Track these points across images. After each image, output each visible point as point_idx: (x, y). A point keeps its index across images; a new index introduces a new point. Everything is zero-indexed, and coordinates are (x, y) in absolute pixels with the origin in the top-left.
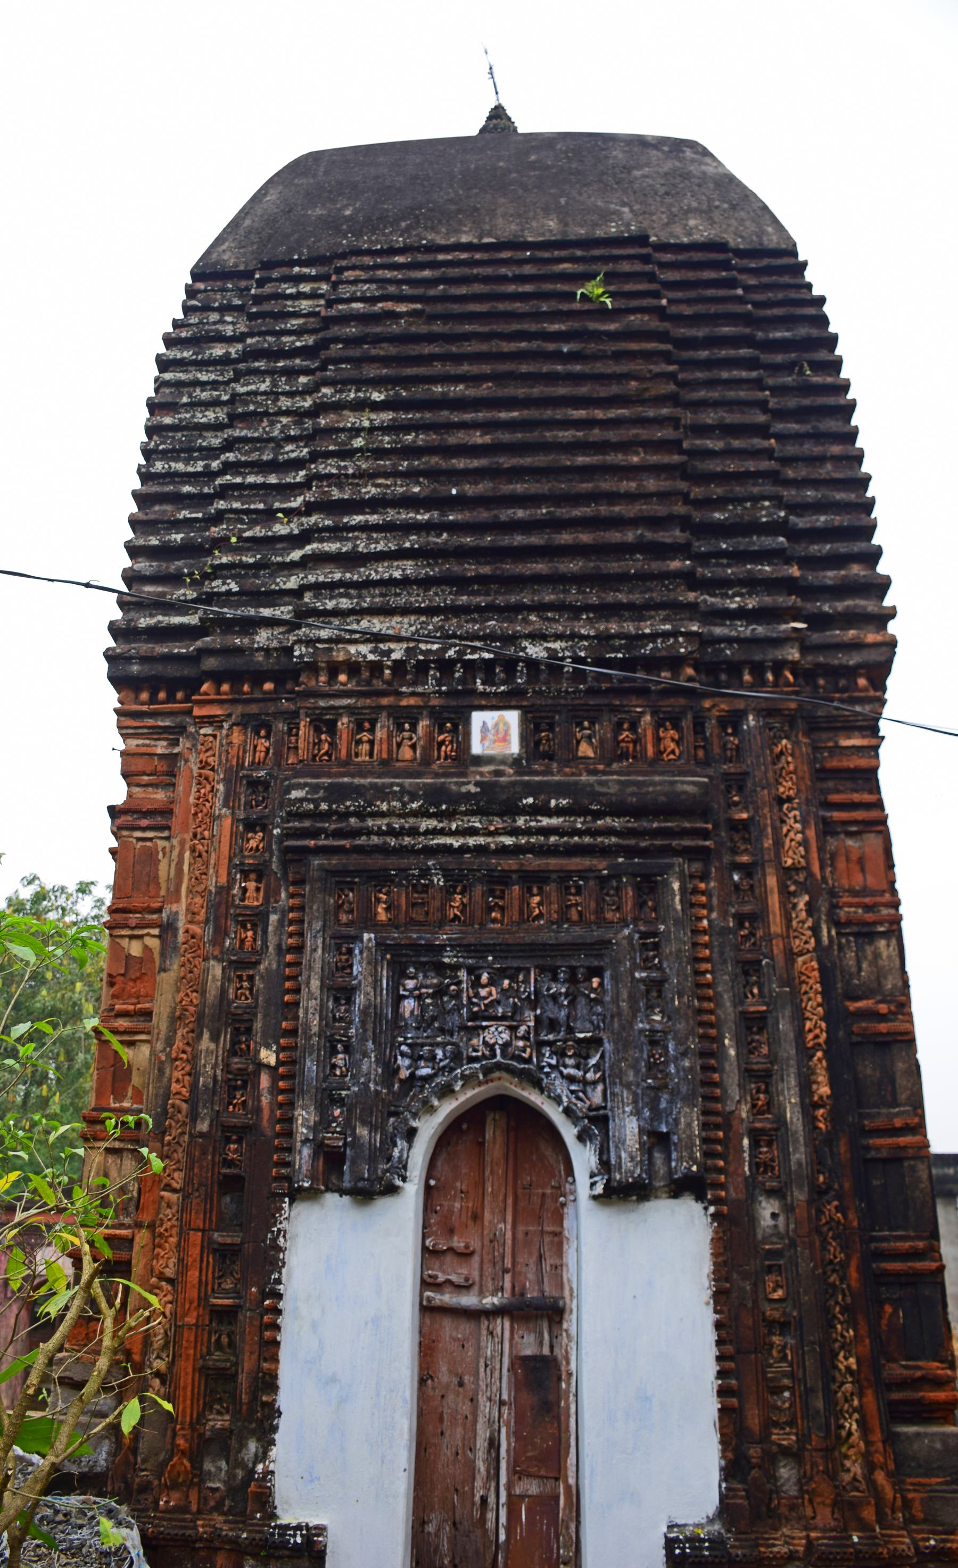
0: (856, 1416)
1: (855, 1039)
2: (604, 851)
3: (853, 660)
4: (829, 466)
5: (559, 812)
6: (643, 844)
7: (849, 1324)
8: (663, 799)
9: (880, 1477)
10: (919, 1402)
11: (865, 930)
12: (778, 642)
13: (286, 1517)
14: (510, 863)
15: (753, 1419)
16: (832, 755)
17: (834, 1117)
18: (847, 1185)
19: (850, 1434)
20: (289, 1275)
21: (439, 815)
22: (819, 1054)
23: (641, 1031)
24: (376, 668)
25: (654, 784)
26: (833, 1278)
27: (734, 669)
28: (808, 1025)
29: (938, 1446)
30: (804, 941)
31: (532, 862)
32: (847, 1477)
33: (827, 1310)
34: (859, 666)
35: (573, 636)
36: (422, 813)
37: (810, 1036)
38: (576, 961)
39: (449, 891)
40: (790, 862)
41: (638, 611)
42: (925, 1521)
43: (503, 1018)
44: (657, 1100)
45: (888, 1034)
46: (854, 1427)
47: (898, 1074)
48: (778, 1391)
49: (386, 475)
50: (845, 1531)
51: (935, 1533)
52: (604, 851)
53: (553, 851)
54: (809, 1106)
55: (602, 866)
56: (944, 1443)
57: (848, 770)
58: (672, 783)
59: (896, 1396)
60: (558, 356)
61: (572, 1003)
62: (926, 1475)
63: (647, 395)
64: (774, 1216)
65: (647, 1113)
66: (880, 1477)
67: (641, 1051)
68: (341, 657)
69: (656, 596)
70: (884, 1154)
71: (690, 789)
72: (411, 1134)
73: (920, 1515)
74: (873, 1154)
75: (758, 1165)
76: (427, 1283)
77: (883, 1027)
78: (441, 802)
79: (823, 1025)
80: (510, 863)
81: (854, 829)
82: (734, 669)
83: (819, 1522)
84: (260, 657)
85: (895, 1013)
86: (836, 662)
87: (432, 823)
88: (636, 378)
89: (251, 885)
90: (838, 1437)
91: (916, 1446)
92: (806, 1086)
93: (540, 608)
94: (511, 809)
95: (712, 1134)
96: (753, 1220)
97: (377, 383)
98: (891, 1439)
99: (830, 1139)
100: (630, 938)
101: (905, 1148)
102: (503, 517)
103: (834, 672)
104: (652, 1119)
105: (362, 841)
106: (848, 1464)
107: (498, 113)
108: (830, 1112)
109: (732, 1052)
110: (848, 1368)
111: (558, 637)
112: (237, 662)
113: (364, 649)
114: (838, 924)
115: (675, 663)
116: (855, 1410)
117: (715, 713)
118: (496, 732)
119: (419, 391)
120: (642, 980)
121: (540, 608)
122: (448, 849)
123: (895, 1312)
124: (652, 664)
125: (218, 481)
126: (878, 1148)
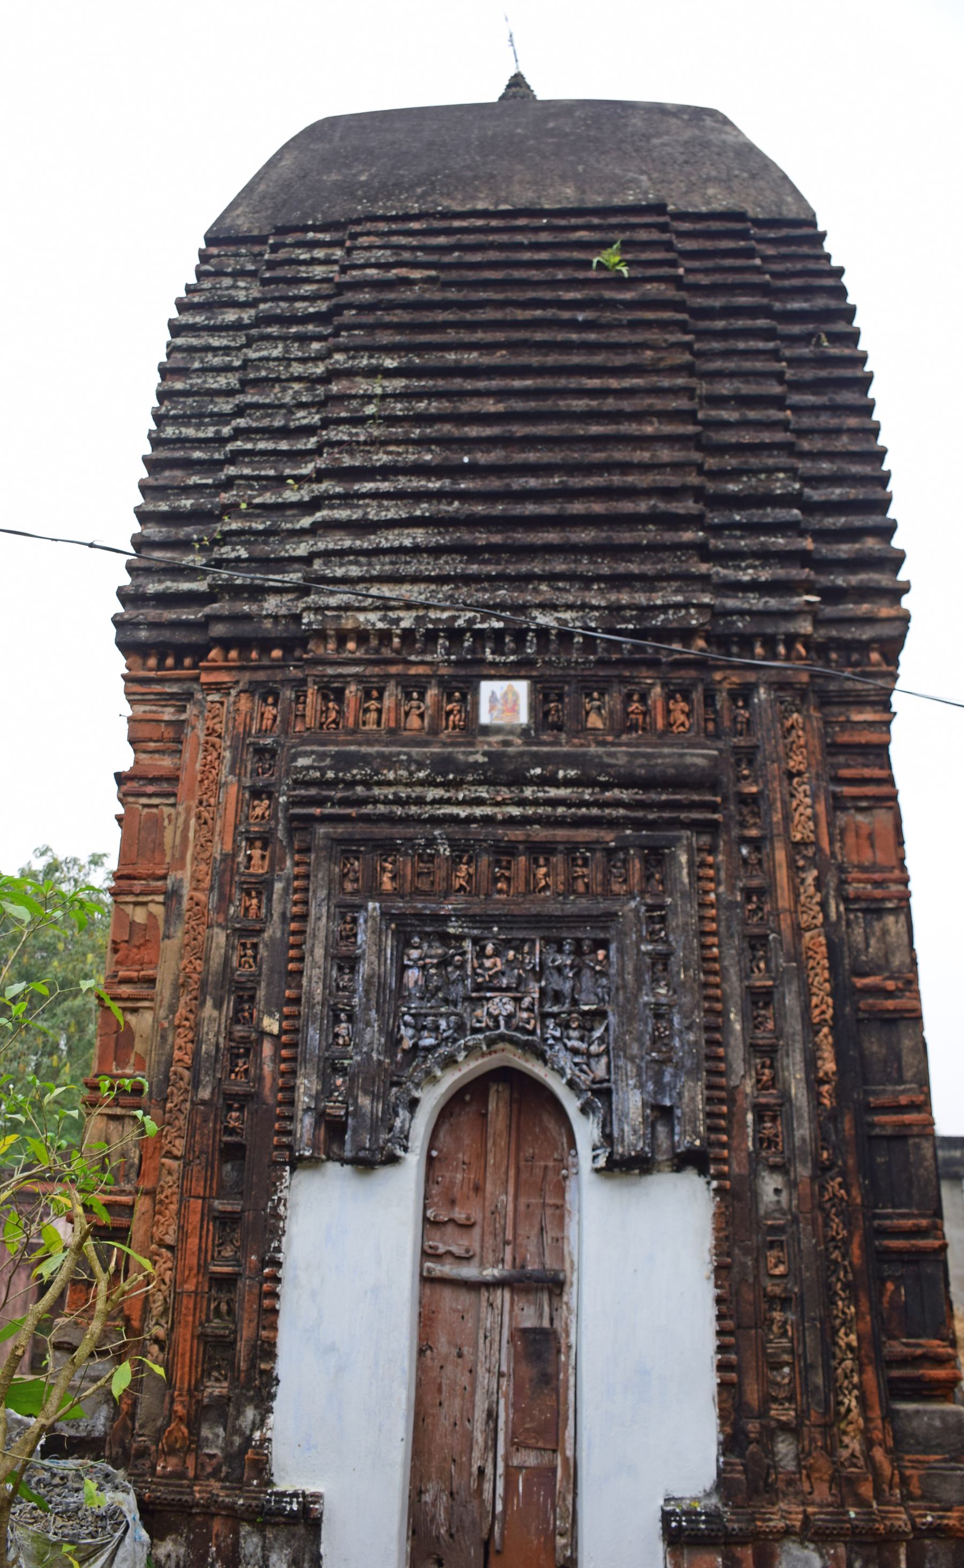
0: (856, 1392)
1: (861, 1015)
2: (612, 823)
3: (866, 634)
5: (567, 783)
9: (878, 1453)
11: (874, 906)
13: (284, 1484)
14: (516, 834)
15: (752, 1395)
17: (840, 1094)
18: (851, 1162)
20: (289, 1243)
21: (446, 785)
22: (825, 1030)
23: (646, 1004)
24: (385, 636)
26: (836, 1255)
27: (746, 642)
28: (815, 1000)
29: (938, 1423)
30: (811, 916)
31: (539, 833)
32: (845, 1453)
35: (583, 606)
36: (428, 783)
37: (817, 1012)
39: (455, 861)
41: (649, 582)
42: (922, 1497)
43: (508, 989)
45: (895, 1011)
46: (854, 1403)
49: (398, 442)
51: (932, 1509)
52: (612, 823)
53: (559, 822)
54: (814, 1082)
55: (609, 837)
58: (682, 755)
59: (895, 1373)
60: (573, 325)
61: (577, 975)
62: (925, 1452)
64: (777, 1191)
66: (878, 1453)
67: (646, 1024)
70: (889, 1131)
71: (700, 761)
72: (413, 1104)
73: (918, 1492)
74: (877, 1131)
75: (761, 1140)
76: (427, 1254)
77: (890, 1004)
78: (447, 771)
80: (516, 834)
81: (864, 804)
83: (816, 1497)
87: (439, 793)
89: (257, 853)
90: (837, 1413)
91: (915, 1423)
92: (811, 1062)
93: (551, 578)
95: (716, 1109)
96: (756, 1195)
97: (389, 349)
98: (890, 1416)
103: (846, 646)
104: (655, 1093)
105: (368, 809)
106: (846, 1440)
108: (836, 1089)
109: (738, 1027)
110: (849, 1346)
111: (569, 607)
112: (245, 629)
114: (846, 900)
115: (686, 635)
116: (855, 1387)
120: (648, 953)
121: (551, 578)
122: (454, 819)
123: (897, 1289)
126: (883, 1126)
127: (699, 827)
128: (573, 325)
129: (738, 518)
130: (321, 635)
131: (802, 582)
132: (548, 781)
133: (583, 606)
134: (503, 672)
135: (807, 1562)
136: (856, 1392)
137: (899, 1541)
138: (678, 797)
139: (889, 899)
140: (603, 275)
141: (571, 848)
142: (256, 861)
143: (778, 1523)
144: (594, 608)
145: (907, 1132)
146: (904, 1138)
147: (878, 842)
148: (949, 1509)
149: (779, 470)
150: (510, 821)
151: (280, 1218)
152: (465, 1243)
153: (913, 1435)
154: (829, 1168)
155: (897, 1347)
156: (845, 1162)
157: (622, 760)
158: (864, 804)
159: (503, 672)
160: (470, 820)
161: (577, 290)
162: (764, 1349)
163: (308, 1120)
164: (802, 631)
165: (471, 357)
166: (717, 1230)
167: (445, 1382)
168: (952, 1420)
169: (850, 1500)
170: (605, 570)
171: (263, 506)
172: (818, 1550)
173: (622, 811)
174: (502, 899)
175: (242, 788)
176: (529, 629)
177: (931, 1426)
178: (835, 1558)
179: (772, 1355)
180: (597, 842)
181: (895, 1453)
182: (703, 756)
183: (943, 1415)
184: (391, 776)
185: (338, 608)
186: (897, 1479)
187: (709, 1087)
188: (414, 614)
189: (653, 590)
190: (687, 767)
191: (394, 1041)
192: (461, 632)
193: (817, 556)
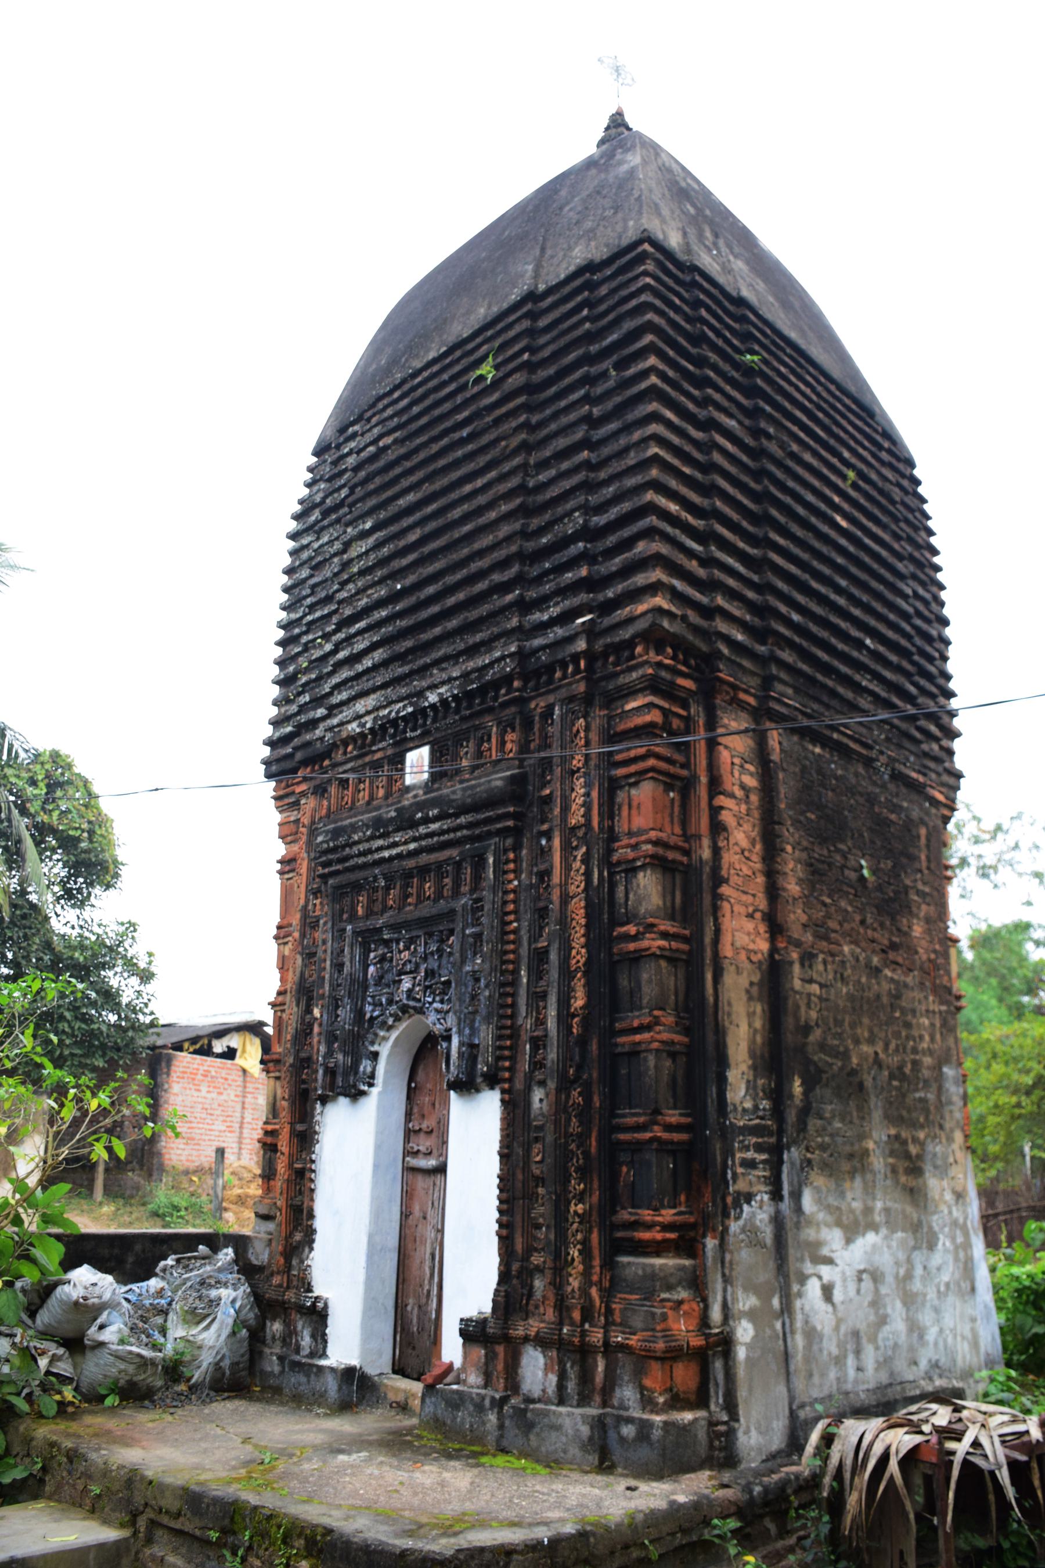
0: (579, 1247)
1: (616, 958)
3: (626, 634)
4: (632, 454)
6: (477, 832)
7: (581, 1179)
8: (469, 800)
9: (594, 1292)
10: (631, 1240)
12: (570, 639)
14: (411, 863)
15: (519, 1246)
16: (621, 719)
17: (585, 1023)
18: (595, 1075)
19: (573, 1259)
20: (321, 1148)
21: (382, 836)
23: (467, 972)
24: (362, 735)
26: (573, 1146)
27: (550, 669)
28: (574, 952)
29: (640, 1272)
30: (577, 885)
31: (424, 859)
32: (569, 1289)
35: (450, 680)
36: (373, 838)
37: (574, 961)
38: (435, 926)
39: (387, 889)
41: (487, 645)
42: (621, 1324)
43: (411, 972)
44: (473, 1021)
45: (635, 951)
46: (576, 1254)
47: (643, 983)
48: (538, 1227)
49: (370, 587)
50: (561, 1324)
51: (624, 1333)
54: (565, 1016)
55: (454, 853)
56: (644, 1270)
57: (630, 730)
58: (489, 782)
59: (619, 1234)
60: (462, 442)
61: (440, 957)
64: (541, 1100)
65: (467, 1031)
66: (594, 1292)
67: (466, 987)
68: (344, 735)
69: (496, 630)
70: (627, 1049)
71: (499, 783)
72: (375, 1055)
73: (618, 1320)
74: (619, 1050)
75: (536, 1063)
76: (408, 1153)
77: (632, 946)
78: (381, 828)
80: (411, 863)
81: (632, 780)
82: (550, 669)
83: (546, 1317)
84: (318, 744)
85: (643, 933)
87: (380, 842)
88: (504, 438)
89: (318, 902)
90: (566, 1260)
91: (627, 1271)
92: (564, 1001)
93: (436, 663)
94: (414, 824)
95: (502, 1043)
96: (528, 1104)
97: (363, 517)
98: (609, 1264)
99: (583, 1042)
100: (464, 906)
101: (639, 1043)
102: (422, 597)
104: (470, 1035)
105: (351, 863)
106: (571, 1279)
107: (617, 122)
108: (582, 1021)
109: (525, 980)
110: (575, 1212)
111: (443, 683)
112: (309, 752)
113: (354, 725)
114: (611, 865)
116: (579, 1242)
117: (539, 710)
118: (418, 762)
119: (392, 510)
121: (436, 663)
122: (383, 860)
123: (628, 1172)
124: (495, 685)
125: (304, 622)
126: (623, 1045)
128: (462, 442)
129: (547, 565)
130: (334, 746)
132: (426, 821)
134: (417, 743)
135: (537, 1359)
136: (579, 1247)
137: (596, 1352)
138: (487, 814)
139: (638, 859)
140: (481, 386)
141: (439, 865)
142: (318, 907)
143: (520, 1332)
145: (639, 1049)
146: (638, 1053)
147: (642, 808)
148: (634, 1334)
149: (574, 510)
150: (412, 854)
151: (316, 1133)
152: (428, 1144)
153: (625, 1280)
154: (573, 1082)
158: (632, 780)
159: (417, 743)
161: (491, 394)
164: (579, 649)
165: (411, 498)
166: (502, 1130)
168: (649, 1270)
169: (567, 1321)
171: (316, 660)
172: (543, 1352)
173: (465, 832)
176: (425, 708)
178: (551, 1358)
179: (535, 1218)
181: (608, 1295)
182: (500, 778)
184: (356, 838)
187: (499, 1028)
188: (372, 716)
190: (492, 789)
191: (360, 1013)
192: (397, 719)
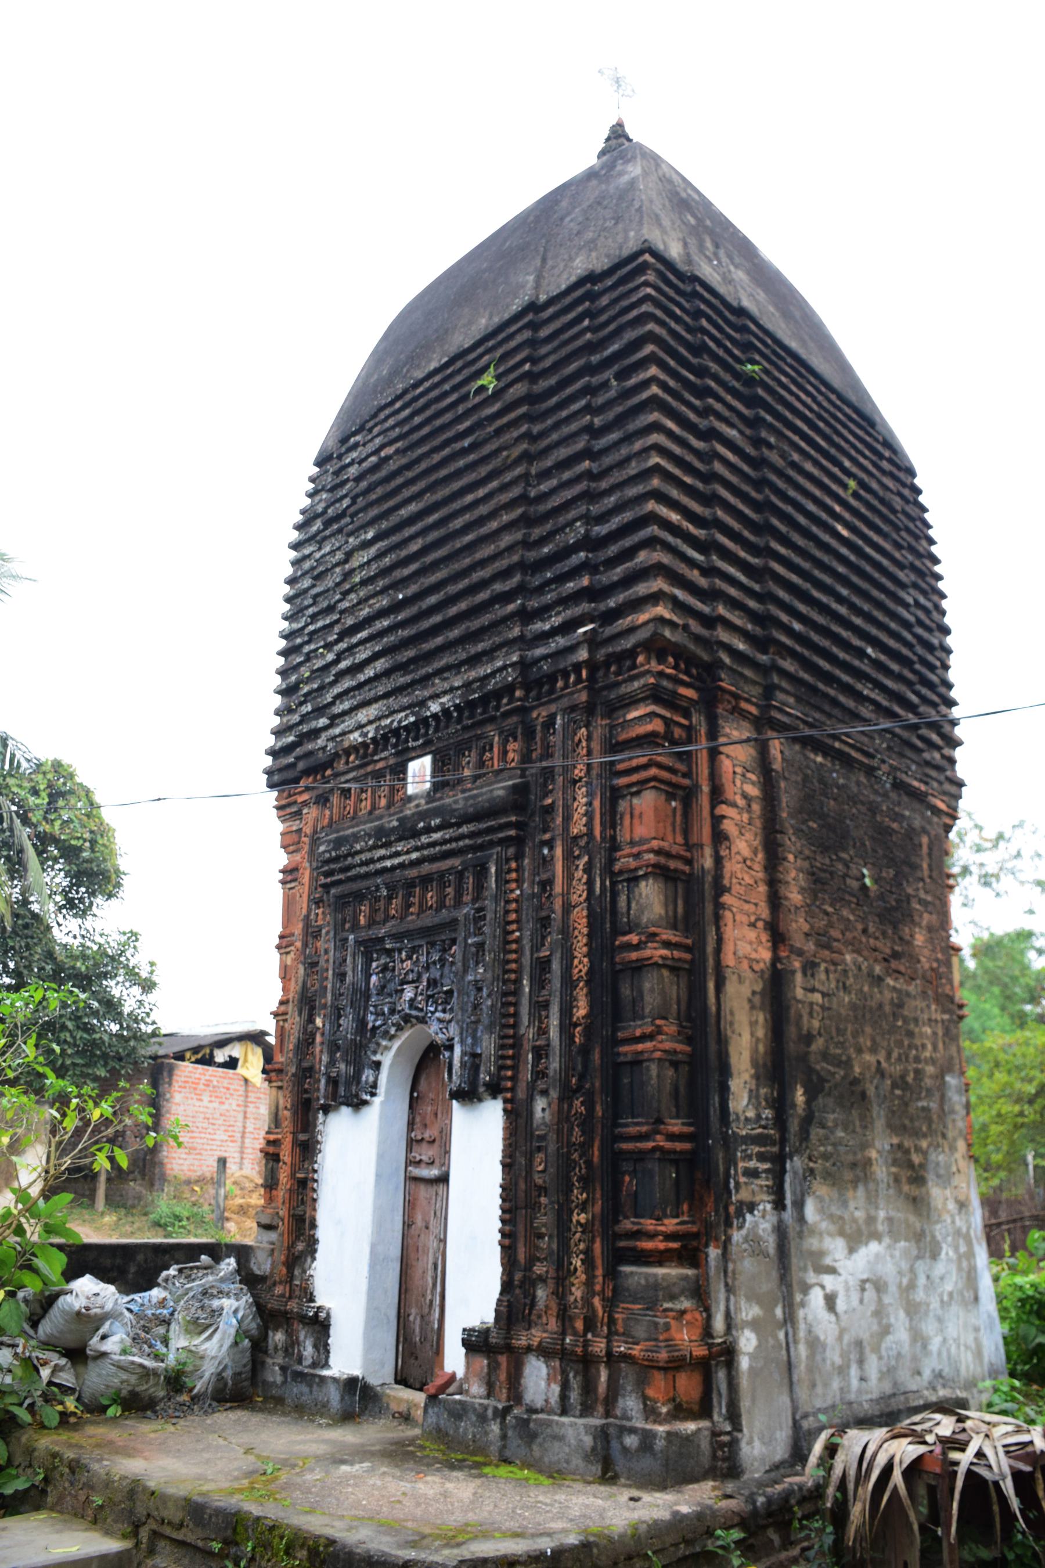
0: (581, 1256)
1: (618, 967)
2: (459, 852)
3: (628, 643)
4: (633, 464)
5: (438, 828)
7: (584, 1189)
8: (471, 810)
9: (597, 1301)
10: (634, 1249)
11: (631, 875)
12: (572, 649)
13: (490, 1318)
14: (413, 873)
15: (521, 1256)
17: (588, 1032)
18: (597, 1084)
19: (576, 1269)
20: (323, 1158)
21: (384, 846)
22: (581, 984)
24: (364, 744)
25: (481, 794)
26: (575, 1156)
28: (576, 962)
29: (643, 1282)
30: (579, 894)
31: (426, 868)
32: (572, 1299)
33: (568, 1179)
34: (636, 646)
35: (452, 689)
36: (375, 847)
37: (576, 971)
38: (437, 936)
39: (390, 898)
40: (575, 831)
41: (488, 654)
42: (624, 1334)
43: (413, 982)
44: (475, 1030)
46: (579, 1263)
47: (646, 992)
48: (541, 1236)
50: (564, 1333)
51: (626, 1343)
52: (459, 852)
53: (432, 859)
54: (567, 1025)
55: (456, 862)
56: (647, 1280)
59: (622, 1244)
61: (442, 966)
62: (633, 1303)
63: (509, 461)
64: (543, 1110)
65: (469, 1041)
66: (597, 1301)
68: (346, 744)
69: (497, 640)
70: (629, 1058)
71: (501, 793)
72: (377, 1065)
73: (621, 1330)
74: (622, 1059)
75: (538, 1072)
76: (410, 1162)
77: (634, 955)
79: (586, 960)
80: (413, 873)
81: (634, 789)
83: (549, 1327)
85: (646, 943)
86: (619, 649)
87: (382, 852)
90: (569, 1270)
91: (630, 1281)
92: (567, 1011)
94: (416, 834)
95: (505, 1052)
96: (531, 1113)
98: (612, 1273)
99: (585, 1051)
101: (642, 1052)
103: (619, 658)
104: (473, 1045)
105: (353, 872)
106: (573, 1289)
109: (527, 990)
110: (578, 1222)
111: (445, 693)
113: (356, 735)
115: (510, 689)
116: (581, 1252)
117: (541, 720)
118: (420, 772)
119: (394, 519)
120: (472, 945)
122: (385, 870)
123: (631, 1181)
124: (497, 694)
126: (625, 1054)
127: (505, 842)
129: (549, 575)
130: (336, 756)
131: (582, 615)
132: (428, 830)
133: (452, 689)
135: (539, 1370)
136: (581, 1256)
140: (483, 396)
142: (320, 917)
144: (458, 688)
145: (641, 1058)
146: (641, 1062)
148: (637, 1344)
151: (318, 1142)
152: (430, 1153)
153: (628, 1290)
154: (576, 1091)
155: (628, 1224)
156: (593, 1084)
157: (460, 805)
158: (634, 789)
159: (419, 752)
160: (393, 868)
162: (532, 1223)
163: (323, 1081)
164: (581, 659)
165: (413, 508)
166: (504, 1139)
167: (420, 1245)
168: (651, 1280)
169: (569, 1331)
170: (464, 656)
172: (546, 1362)
173: (467, 841)
174: (414, 921)
175: (313, 870)
177: (639, 1283)
178: (554, 1368)
179: (537, 1228)
180: (452, 868)
181: (610, 1304)
183: (647, 1276)
184: (358, 847)
185: (341, 735)
186: (606, 1320)
189: (493, 659)
190: (494, 799)
191: (362, 1023)
193: (598, 587)
